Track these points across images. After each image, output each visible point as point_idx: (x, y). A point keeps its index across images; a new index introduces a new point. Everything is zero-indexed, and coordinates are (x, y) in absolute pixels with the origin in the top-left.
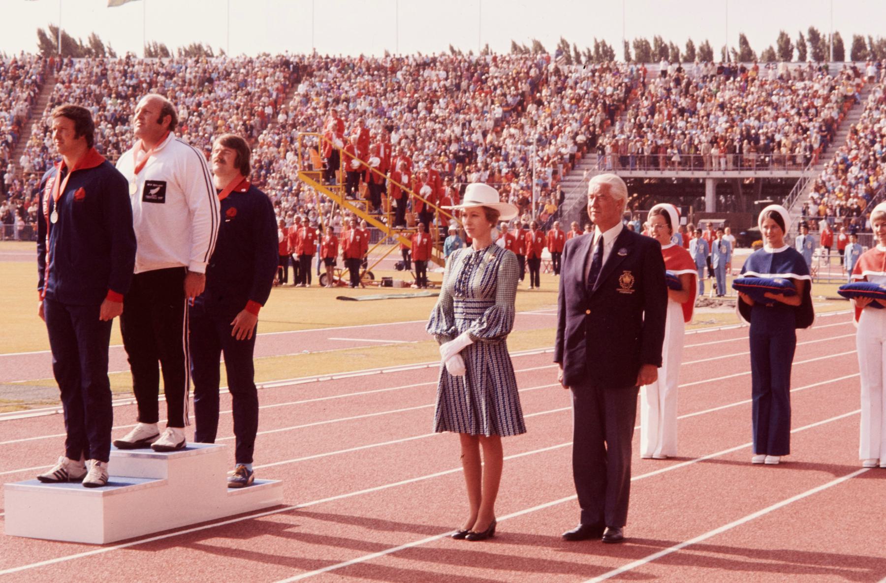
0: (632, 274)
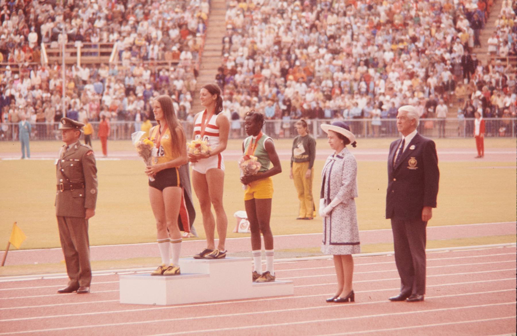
0: (416, 159)
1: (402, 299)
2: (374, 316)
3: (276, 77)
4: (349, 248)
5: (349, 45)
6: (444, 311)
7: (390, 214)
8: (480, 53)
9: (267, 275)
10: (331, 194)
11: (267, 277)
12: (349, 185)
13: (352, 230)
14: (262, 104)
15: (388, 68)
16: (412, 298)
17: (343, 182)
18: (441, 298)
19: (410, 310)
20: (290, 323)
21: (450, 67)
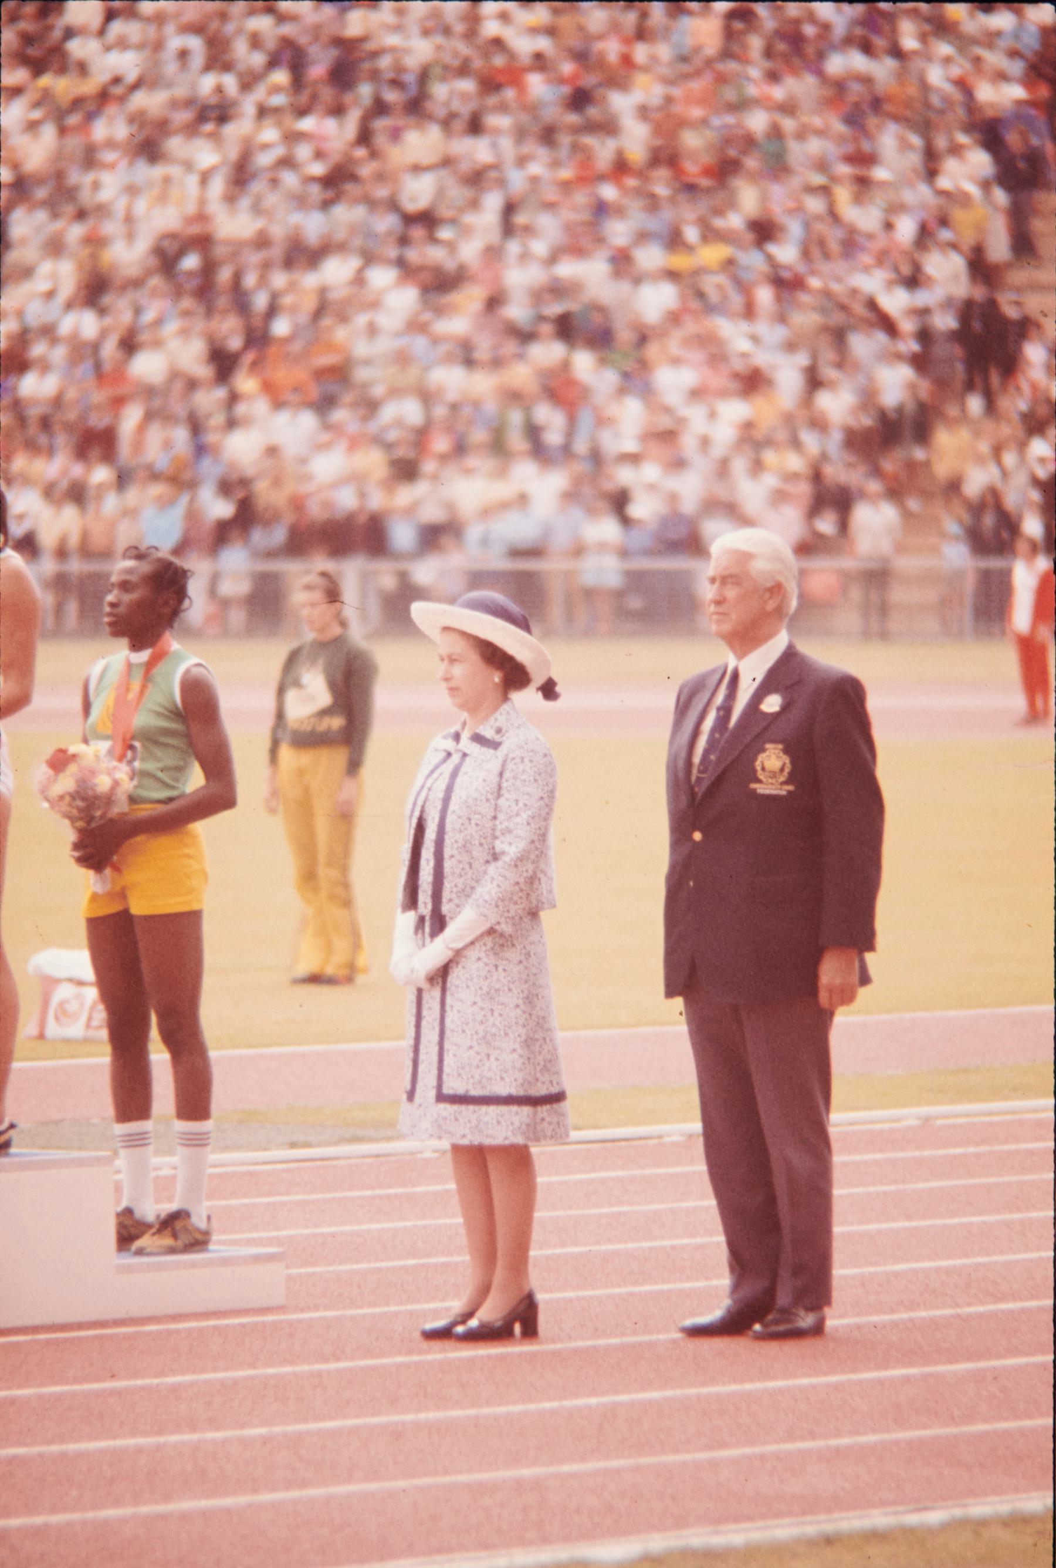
0: (786, 751)
1: (733, 1325)
2: (623, 1398)
3: (192, 384)
4: (517, 1121)
5: (493, 254)
6: (907, 1379)
7: (684, 976)
8: (1036, 287)
9: (178, 1225)
10: (446, 895)
11: (179, 1231)
12: (521, 859)
13: (528, 1042)
14: (133, 495)
15: (652, 351)
16: (777, 1322)
17: (499, 846)
18: (895, 1325)
19: (768, 1375)
20: (277, 1429)
21: (915, 347)
